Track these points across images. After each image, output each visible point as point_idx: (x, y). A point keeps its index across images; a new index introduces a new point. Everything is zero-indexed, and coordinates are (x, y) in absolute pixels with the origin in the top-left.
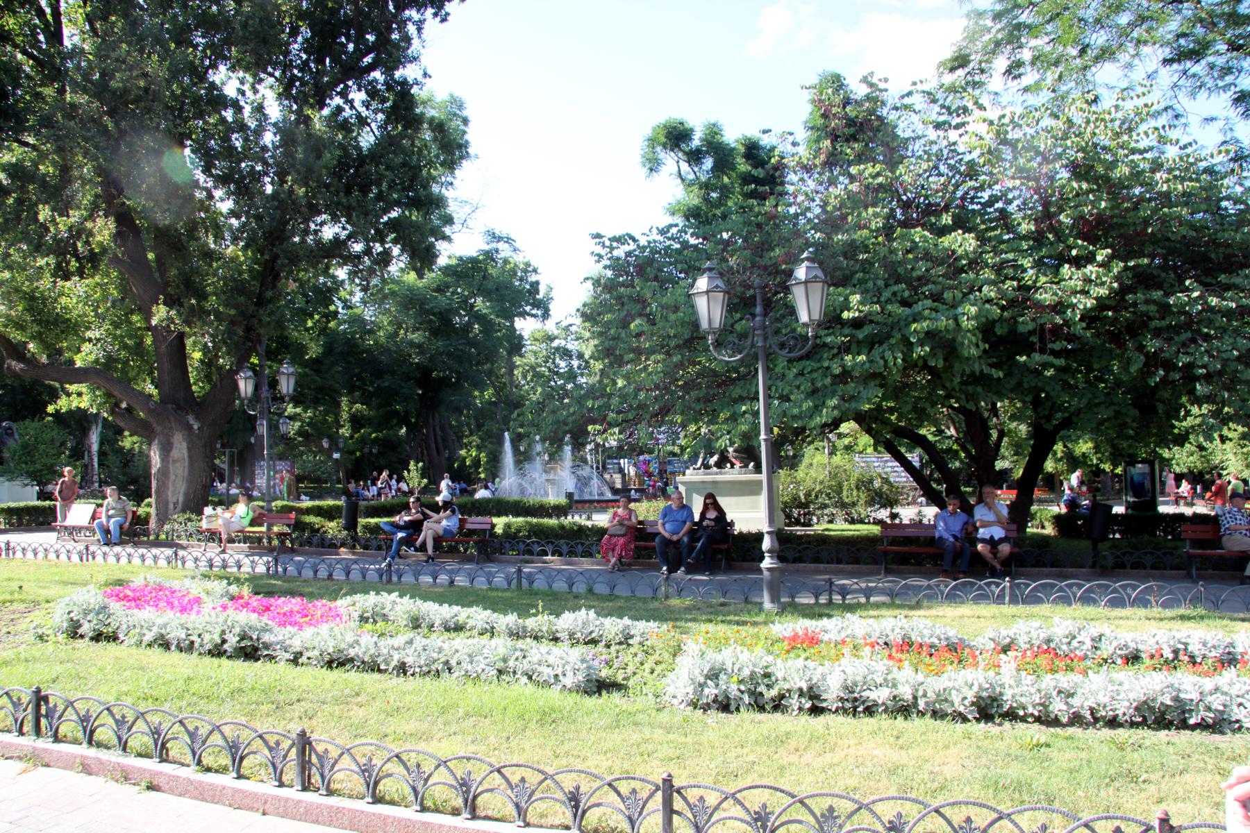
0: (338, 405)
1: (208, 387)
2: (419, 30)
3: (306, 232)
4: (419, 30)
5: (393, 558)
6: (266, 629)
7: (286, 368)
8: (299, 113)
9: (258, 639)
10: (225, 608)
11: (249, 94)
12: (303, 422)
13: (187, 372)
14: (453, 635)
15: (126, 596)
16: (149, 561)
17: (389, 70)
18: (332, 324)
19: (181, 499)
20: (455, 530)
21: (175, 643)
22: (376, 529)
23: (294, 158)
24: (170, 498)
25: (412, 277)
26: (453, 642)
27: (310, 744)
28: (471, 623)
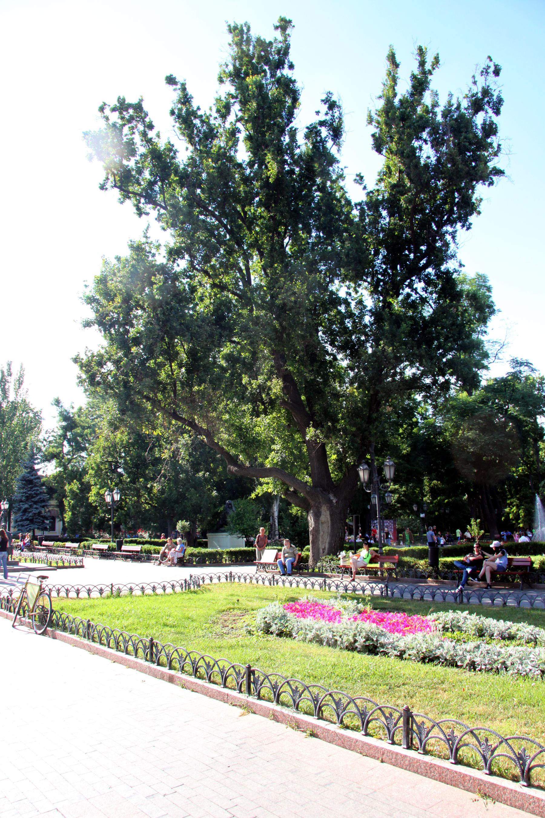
0: (422, 482)
1: (340, 475)
2: (453, 238)
3: (395, 374)
4: (453, 238)
5: (463, 585)
6: (382, 635)
7: (388, 462)
8: (384, 301)
9: (377, 641)
10: (355, 619)
11: (353, 294)
12: (400, 494)
13: (328, 466)
14: (507, 642)
15: (296, 609)
16: (309, 586)
17: (437, 266)
18: (415, 430)
19: (327, 546)
20: (505, 566)
21: (326, 640)
22: (450, 566)
23: (383, 330)
24: (320, 546)
25: (464, 395)
26: (508, 648)
27: (412, 717)
28: (520, 634)
